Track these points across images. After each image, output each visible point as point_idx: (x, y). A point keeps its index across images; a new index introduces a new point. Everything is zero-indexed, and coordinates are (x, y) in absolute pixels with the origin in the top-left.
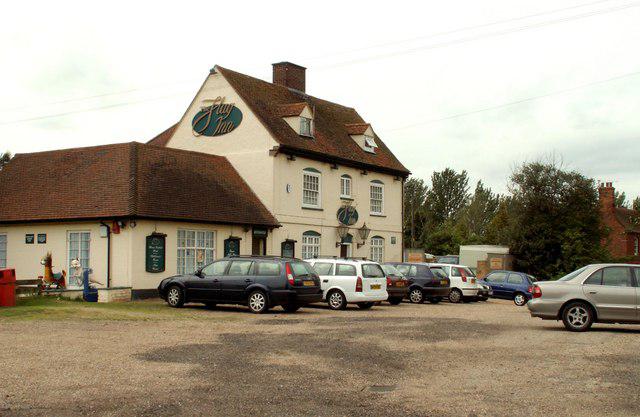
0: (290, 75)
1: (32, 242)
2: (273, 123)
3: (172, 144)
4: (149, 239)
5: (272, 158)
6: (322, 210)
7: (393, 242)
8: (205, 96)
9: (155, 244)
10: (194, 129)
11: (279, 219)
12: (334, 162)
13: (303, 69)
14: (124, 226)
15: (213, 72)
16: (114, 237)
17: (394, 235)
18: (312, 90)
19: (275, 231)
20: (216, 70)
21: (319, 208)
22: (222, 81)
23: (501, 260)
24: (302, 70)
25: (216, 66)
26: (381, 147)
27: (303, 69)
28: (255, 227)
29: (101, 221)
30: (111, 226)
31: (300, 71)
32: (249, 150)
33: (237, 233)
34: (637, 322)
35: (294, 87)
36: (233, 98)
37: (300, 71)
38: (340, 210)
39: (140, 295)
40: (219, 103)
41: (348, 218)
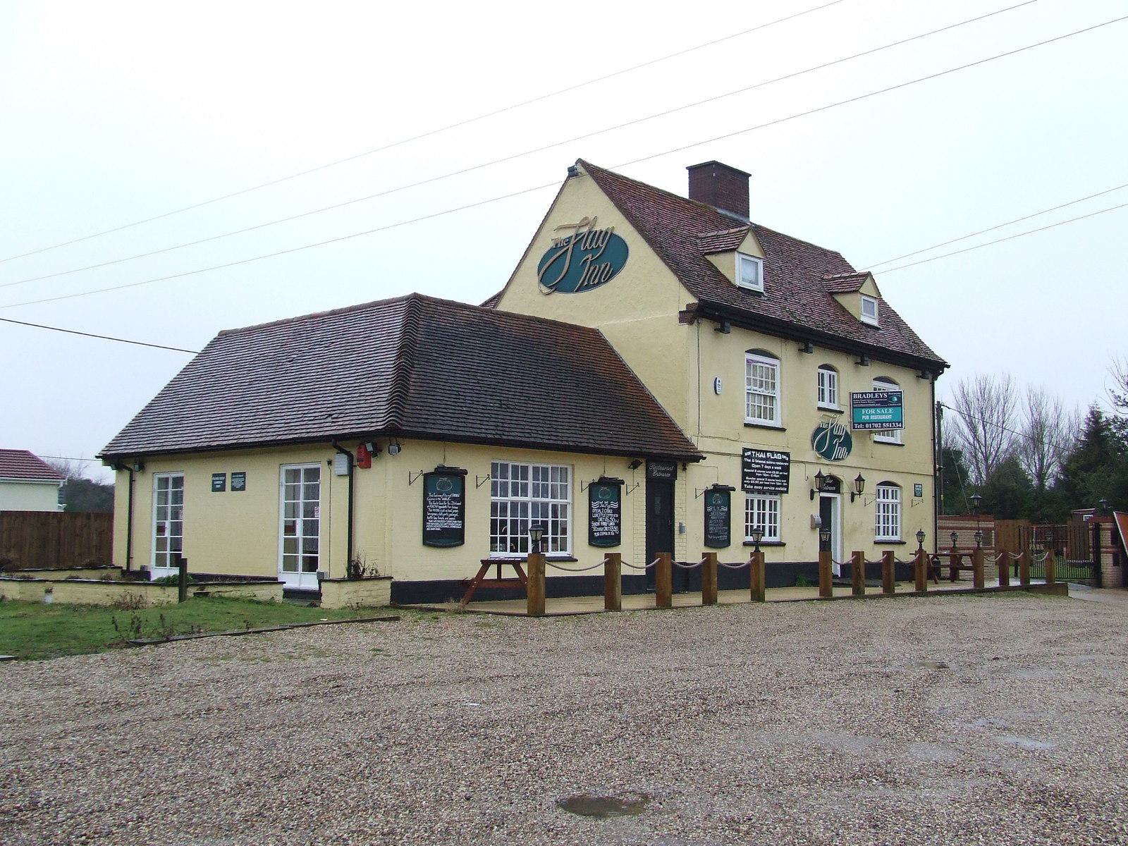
0: (721, 187)
1: (223, 489)
2: (691, 265)
3: (504, 307)
4: (430, 480)
5: (686, 326)
6: (783, 430)
7: (918, 494)
8: (558, 219)
9: (444, 486)
10: (541, 281)
11: (701, 445)
12: (805, 338)
13: (747, 176)
14: (377, 452)
15: (572, 172)
16: (361, 475)
17: (919, 480)
18: (760, 213)
19: (693, 468)
20: (580, 169)
21: (779, 425)
22: (590, 184)
23: (960, 578)
24: (745, 176)
25: (580, 161)
26: (889, 316)
27: (747, 176)
28: (651, 459)
29: (337, 442)
30: (354, 453)
31: (741, 179)
32: (639, 312)
33: (615, 470)
34: (2, 479)
35: (727, 208)
36: (610, 219)
37: (741, 179)
38: (819, 430)
39: (411, 596)
40: (585, 230)
41: (832, 447)
